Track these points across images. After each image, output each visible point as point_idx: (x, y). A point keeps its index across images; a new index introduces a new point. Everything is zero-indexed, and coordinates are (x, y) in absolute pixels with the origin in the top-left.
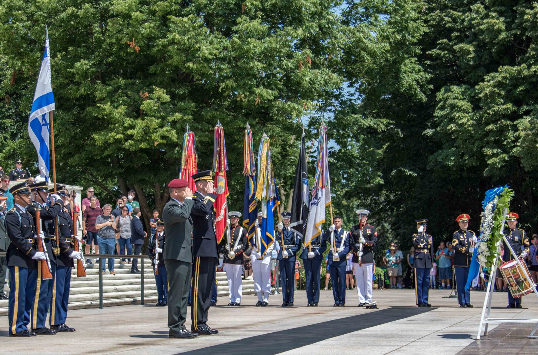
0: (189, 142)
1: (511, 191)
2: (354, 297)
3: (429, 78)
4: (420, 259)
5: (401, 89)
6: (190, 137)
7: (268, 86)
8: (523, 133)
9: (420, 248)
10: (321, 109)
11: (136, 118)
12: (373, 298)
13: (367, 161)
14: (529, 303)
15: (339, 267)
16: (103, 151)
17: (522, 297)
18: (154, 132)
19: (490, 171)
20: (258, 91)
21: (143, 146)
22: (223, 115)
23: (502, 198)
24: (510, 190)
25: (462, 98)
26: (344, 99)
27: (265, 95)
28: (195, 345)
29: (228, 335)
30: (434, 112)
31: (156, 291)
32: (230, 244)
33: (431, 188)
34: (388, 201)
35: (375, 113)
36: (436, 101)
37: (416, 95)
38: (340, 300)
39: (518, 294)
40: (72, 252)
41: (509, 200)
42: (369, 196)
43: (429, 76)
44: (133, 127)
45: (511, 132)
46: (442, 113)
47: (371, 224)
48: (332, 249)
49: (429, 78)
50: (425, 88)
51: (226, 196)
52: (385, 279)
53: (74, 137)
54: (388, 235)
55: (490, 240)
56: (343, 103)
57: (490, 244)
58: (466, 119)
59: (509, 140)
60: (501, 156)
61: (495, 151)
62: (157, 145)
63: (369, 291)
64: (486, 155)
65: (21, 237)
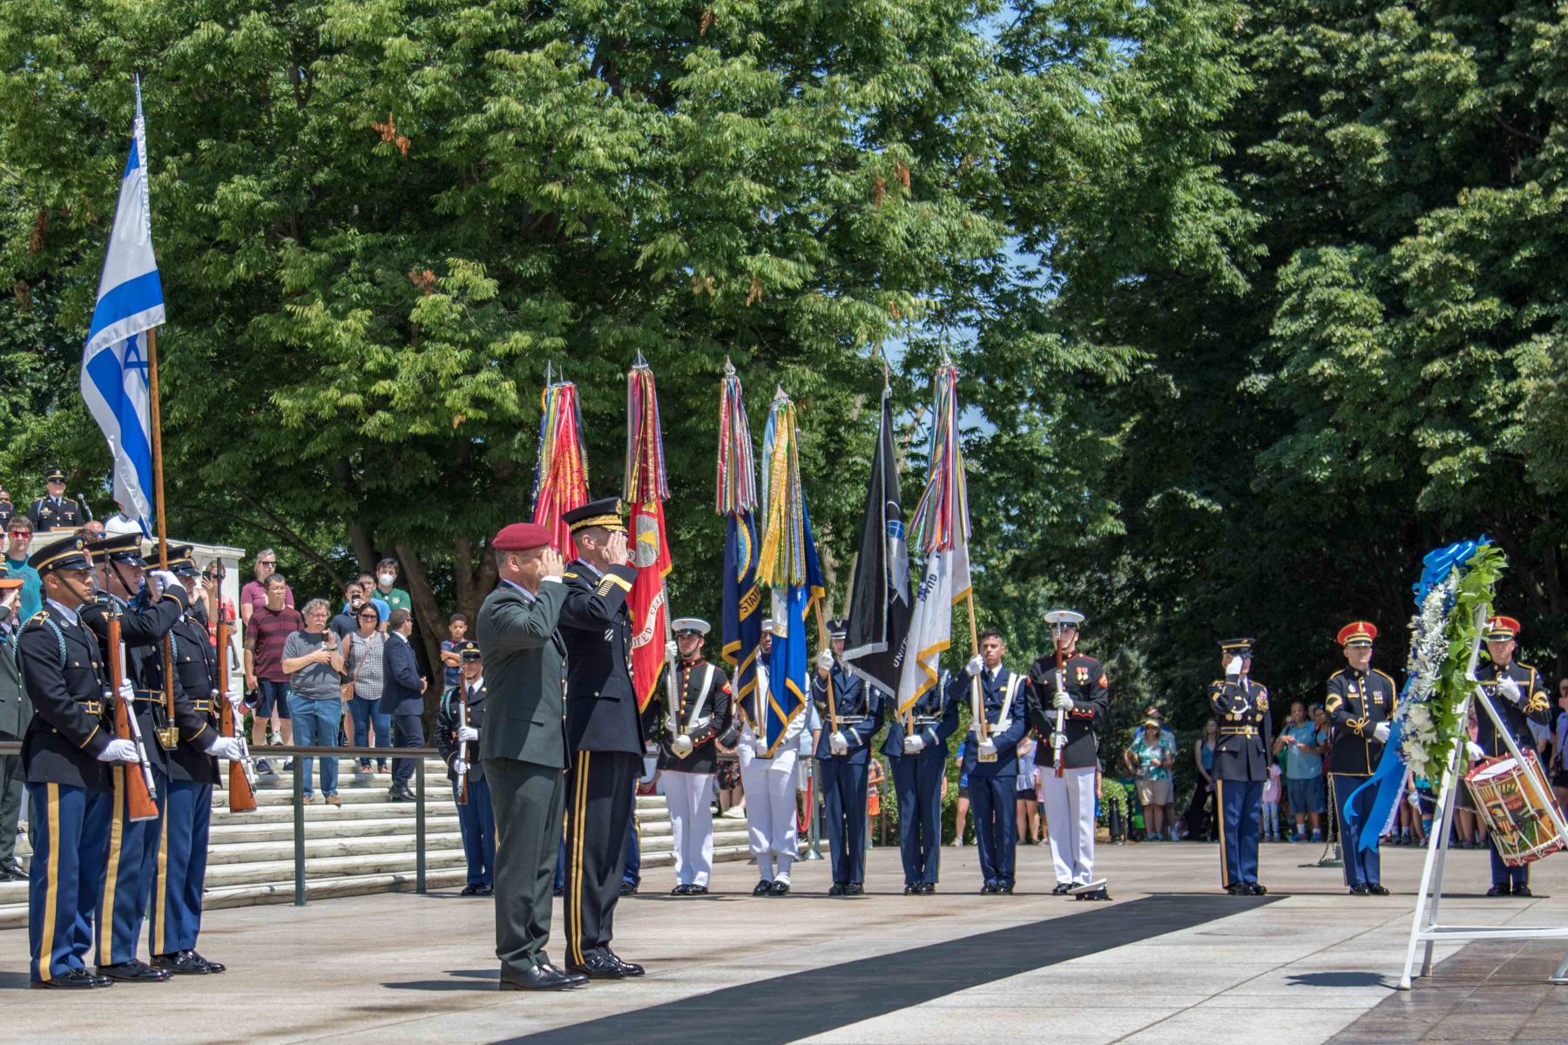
1: (1499, 554)
2: (1040, 866)
3: (1255, 226)
4: (1234, 754)
5: (1173, 257)
6: (564, 396)
7: (786, 252)
8: (1530, 386)
9: (1234, 723)
10: (940, 317)
11: (399, 345)
12: (1095, 868)
13: (1075, 468)
14: (1551, 880)
15: (997, 778)
16: (302, 444)
17: (1532, 865)
18: (450, 387)
19: (1437, 495)
20: (753, 263)
21: (418, 428)
23: (1473, 574)
24: (1496, 550)
25: (1353, 282)
26: (1006, 287)
27: (776, 275)
28: (577, 1009)
29: (673, 980)
30: (1270, 324)
31: (461, 853)
33: (1262, 548)
34: (1138, 585)
35: (1097, 328)
36: (1277, 292)
37: (1218, 274)
38: (999, 876)
39: (1519, 855)
41: (1492, 580)
42: (1082, 571)
43: (1254, 220)
44: (389, 372)
45: (1496, 382)
46: (1293, 327)
47: (1087, 652)
48: (976, 726)
49: (1255, 226)
50: (1244, 255)
51: (663, 575)
52: (1130, 813)
54: (1140, 685)
55: (1438, 696)
56: (1005, 299)
57: (1439, 709)
58: (1366, 346)
59: (1492, 406)
60: (1468, 451)
61: (1451, 437)
62: (461, 423)
63: (1085, 850)
64: (1424, 449)
65: (67, 698)
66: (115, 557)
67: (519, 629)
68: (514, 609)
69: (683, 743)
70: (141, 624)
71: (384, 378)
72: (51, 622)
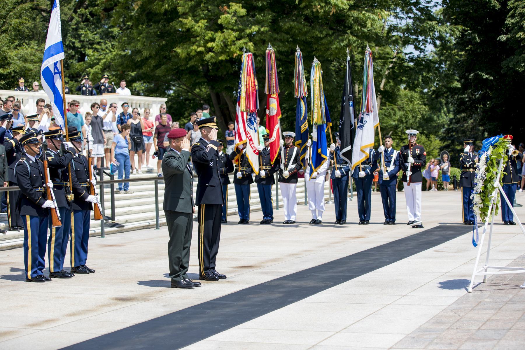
0: (248, 63)
4: (467, 178)
6: (249, 57)
9: (467, 168)
11: (216, 31)
16: (187, 63)
21: (222, 58)
22: (300, 25)
26: (421, 6)
32: (284, 164)
35: (453, 19)
40: (87, 197)
44: (213, 40)
46: (512, 21)
51: (279, 118)
53: (162, 48)
55: (483, 192)
57: (484, 196)
65: (30, 187)
66: (52, 137)
67: (173, 168)
68: (173, 160)
69: (286, 174)
70: (60, 161)
71: (211, 42)
72: (26, 162)
